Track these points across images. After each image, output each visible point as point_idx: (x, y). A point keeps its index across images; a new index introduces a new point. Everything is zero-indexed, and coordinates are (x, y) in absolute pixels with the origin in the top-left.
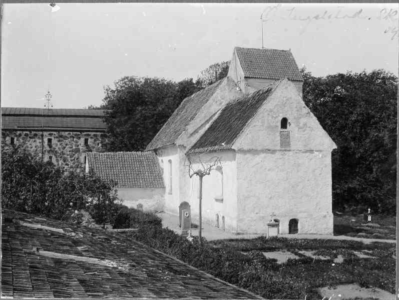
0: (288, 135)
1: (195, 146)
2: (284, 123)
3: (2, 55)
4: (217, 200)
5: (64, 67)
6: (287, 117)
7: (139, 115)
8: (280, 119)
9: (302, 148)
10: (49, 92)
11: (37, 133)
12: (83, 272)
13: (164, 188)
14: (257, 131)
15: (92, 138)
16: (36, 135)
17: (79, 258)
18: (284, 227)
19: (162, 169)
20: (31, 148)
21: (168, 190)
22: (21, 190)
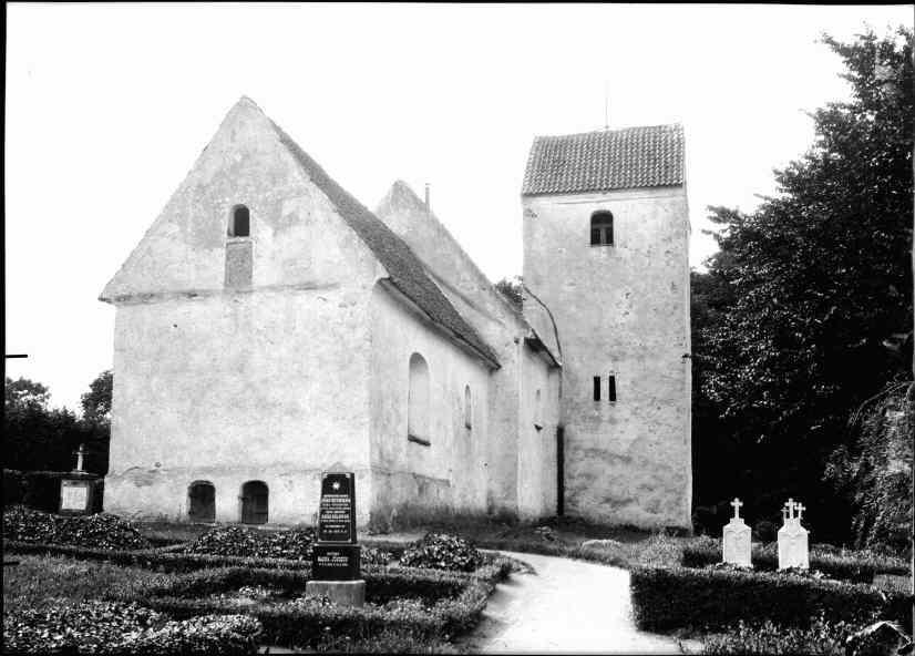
0: (246, 254)
2: (241, 222)
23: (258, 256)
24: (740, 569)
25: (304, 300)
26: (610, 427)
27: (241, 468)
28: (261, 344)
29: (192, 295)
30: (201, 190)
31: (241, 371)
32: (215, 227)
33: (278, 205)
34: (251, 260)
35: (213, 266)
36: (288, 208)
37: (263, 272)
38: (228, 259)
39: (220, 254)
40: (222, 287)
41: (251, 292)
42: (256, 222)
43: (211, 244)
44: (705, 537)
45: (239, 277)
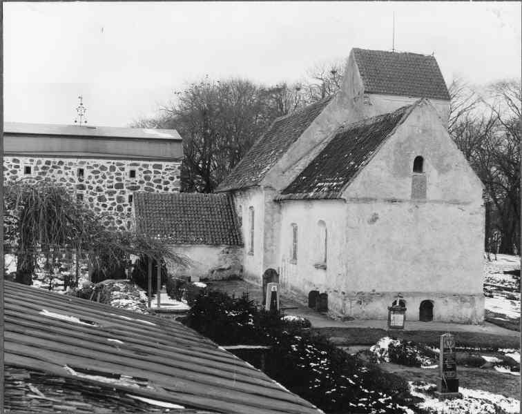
0: (423, 182)
1: (286, 191)
2: (419, 163)
3: (381, 2)
4: (317, 266)
5: (98, 77)
6: (423, 156)
7: (222, 140)
8: (413, 159)
9: (438, 196)
10: (81, 104)
11: (63, 160)
12: (149, 387)
13: (242, 245)
14: (378, 169)
15: (140, 169)
16: (61, 163)
17: (429, 367)
18: (413, 309)
19: (241, 219)
20: (55, 181)
21: (248, 247)
22: (429, 220)
23: (430, 184)
24: (347, 318)
25: (453, 209)
26: (445, 405)
27: (420, 294)
28: (317, 68)
29: (393, 201)
30: (399, 145)
31: (486, 320)
32: (407, 165)
33: (441, 159)
34: (426, 186)
35: (406, 186)
36: (447, 160)
37: (432, 192)
38: (413, 184)
39: (409, 181)
40: (410, 198)
41: (426, 202)
42: (428, 165)
43: (405, 175)
44: (80, 288)
45: (419, 192)
